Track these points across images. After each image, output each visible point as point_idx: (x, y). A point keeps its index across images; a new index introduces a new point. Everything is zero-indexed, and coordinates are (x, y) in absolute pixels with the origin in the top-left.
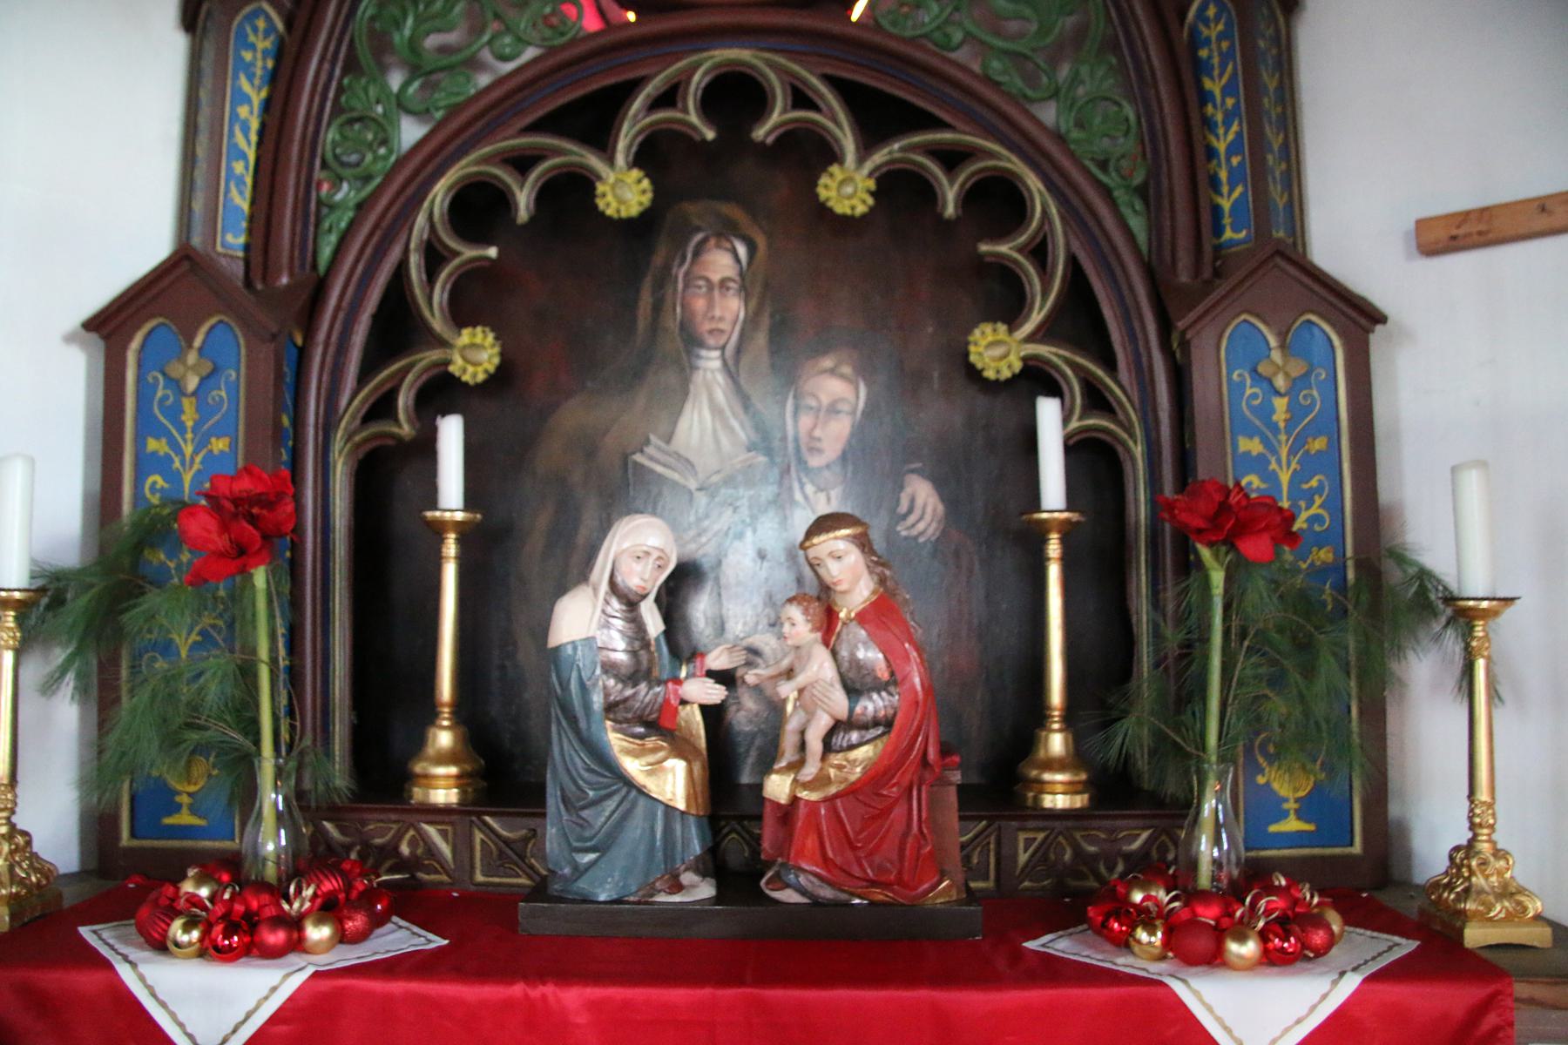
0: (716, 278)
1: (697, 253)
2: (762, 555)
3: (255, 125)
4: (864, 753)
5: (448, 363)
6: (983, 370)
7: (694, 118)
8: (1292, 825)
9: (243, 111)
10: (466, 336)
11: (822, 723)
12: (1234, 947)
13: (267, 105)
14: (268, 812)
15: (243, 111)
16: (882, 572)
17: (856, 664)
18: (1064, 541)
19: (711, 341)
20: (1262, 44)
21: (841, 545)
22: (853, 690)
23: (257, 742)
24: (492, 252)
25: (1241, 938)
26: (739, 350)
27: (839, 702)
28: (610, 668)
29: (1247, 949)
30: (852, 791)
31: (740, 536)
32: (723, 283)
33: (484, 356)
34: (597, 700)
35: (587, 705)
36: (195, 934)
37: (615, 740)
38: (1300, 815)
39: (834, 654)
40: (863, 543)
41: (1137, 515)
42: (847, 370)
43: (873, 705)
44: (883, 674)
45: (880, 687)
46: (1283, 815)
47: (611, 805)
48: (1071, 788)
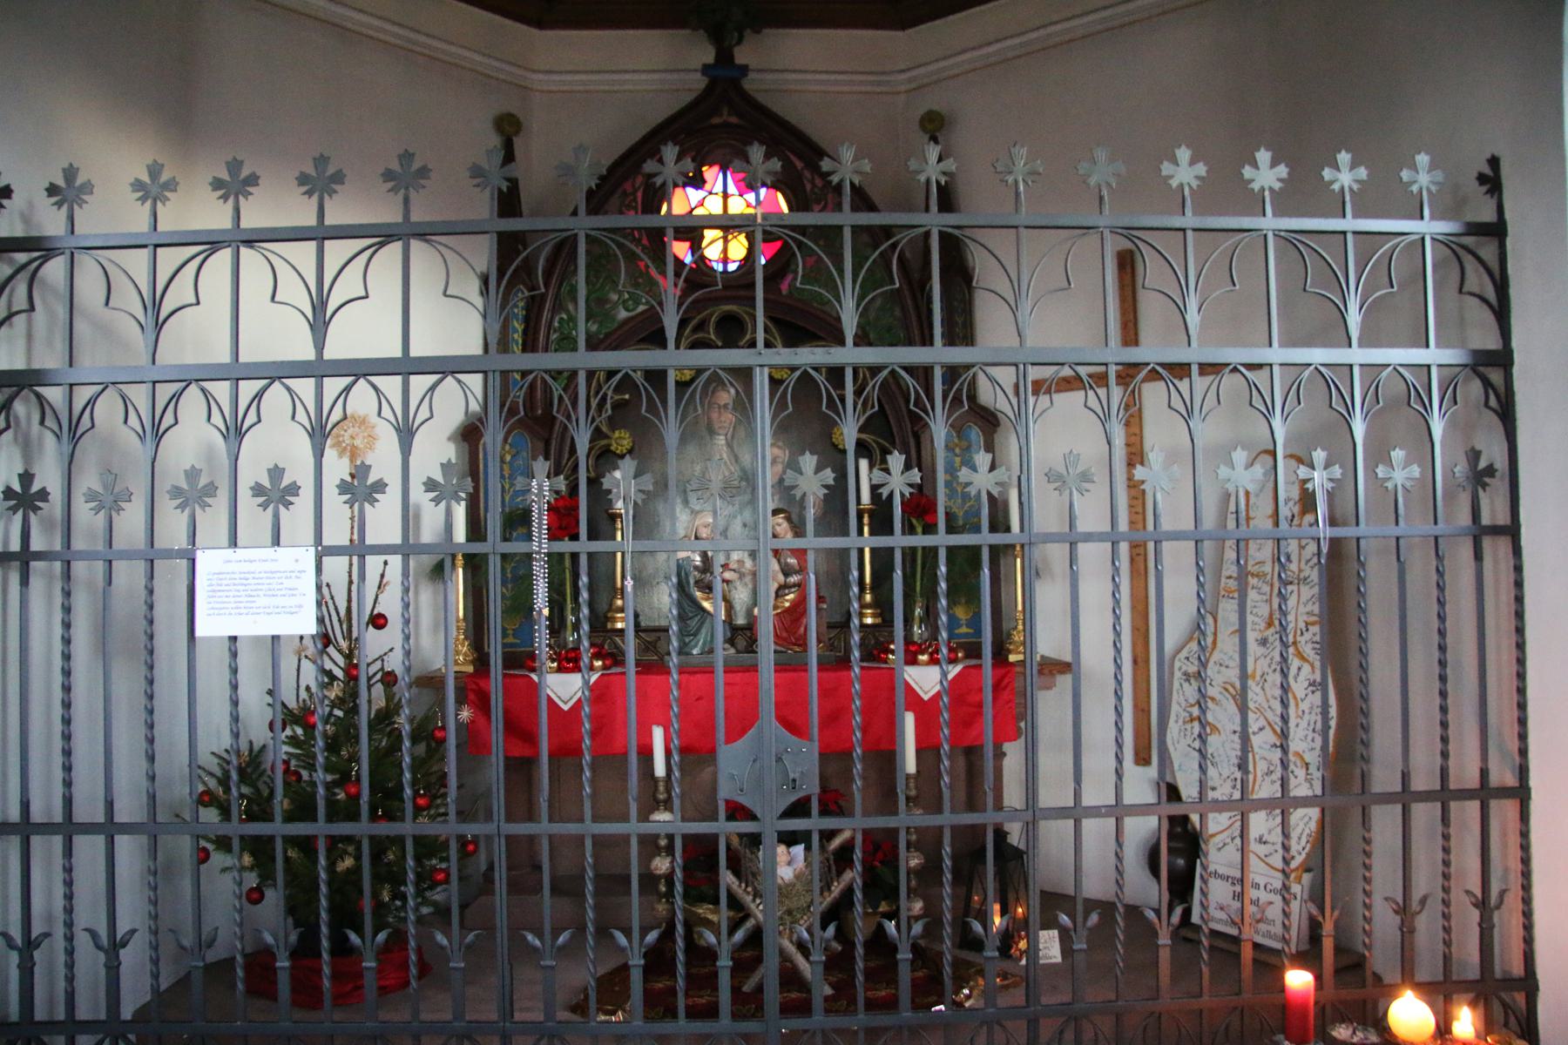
0: (722, 403)
1: (713, 392)
2: (745, 525)
3: (520, 341)
4: (791, 596)
5: (610, 445)
6: (826, 487)
7: (713, 337)
8: (964, 630)
9: (516, 336)
10: (617, 434)
11: (776, 586)
12: (920, 657)
13: (525, 332)
14: (569, 624)
15: (516, 336)
16: (862, 449)
17: (787, 564)
18: (870, 517)
19: (721, 432)
20: (956, 304)
21: (780, 521)
22: (786, 574)
23: (565, 600)
24: (627, 397)
25: (923, 654)
26: (733, 437)
27: (781, 578)
28: (696, 568)
29: (924, 658)
30: (787, 610)
31: (735, 517)
32: (726, 406)
33: (625, 442)
34: (692, 581)
35: (688, 583)
36: (555, 664)
37: (698, 594)
38: (968, 626)
39: (779, 561)
40: (789, 519)
41: (1496, 562)
42: (780, 444)
43: (794, 579)
44: (797, 568)
45: (796, 572)
46: (960, 626)
47: (696, 619)
48: (873, 616)
